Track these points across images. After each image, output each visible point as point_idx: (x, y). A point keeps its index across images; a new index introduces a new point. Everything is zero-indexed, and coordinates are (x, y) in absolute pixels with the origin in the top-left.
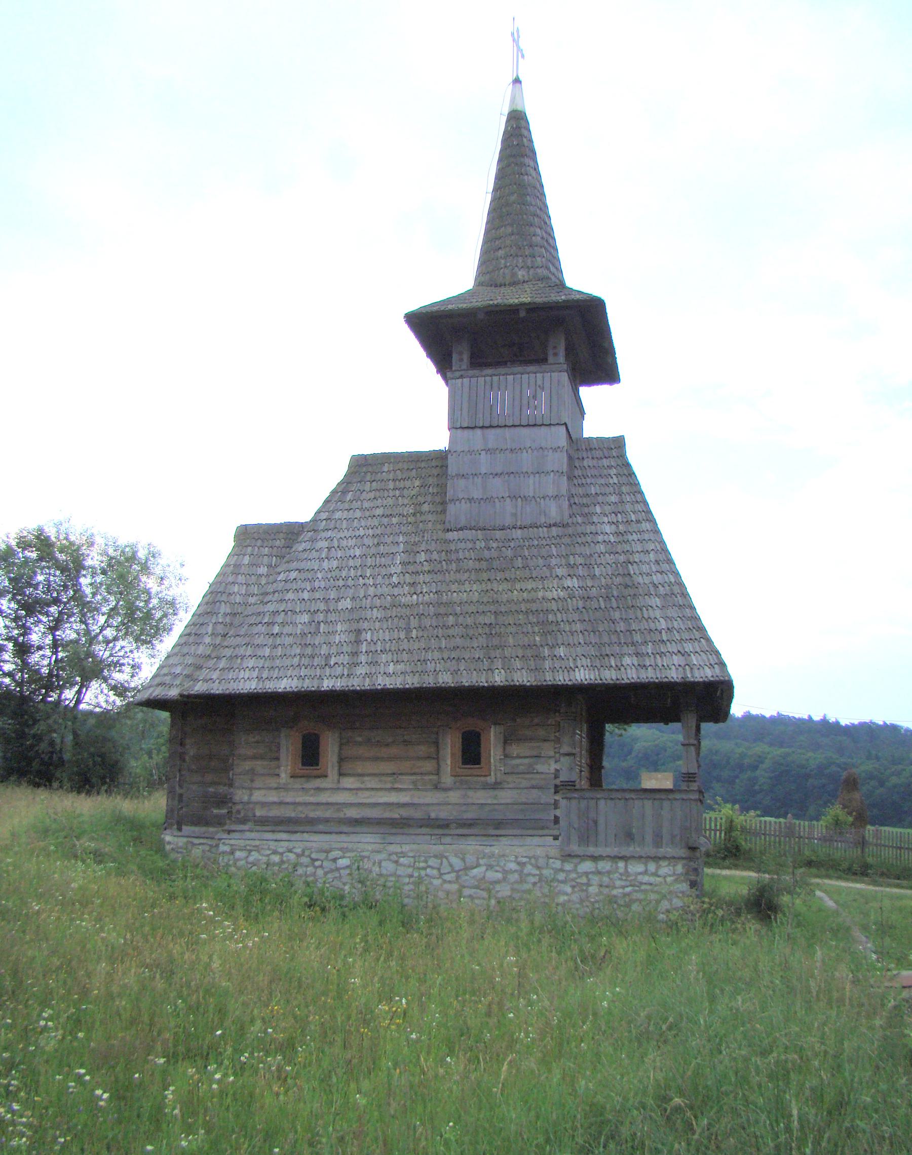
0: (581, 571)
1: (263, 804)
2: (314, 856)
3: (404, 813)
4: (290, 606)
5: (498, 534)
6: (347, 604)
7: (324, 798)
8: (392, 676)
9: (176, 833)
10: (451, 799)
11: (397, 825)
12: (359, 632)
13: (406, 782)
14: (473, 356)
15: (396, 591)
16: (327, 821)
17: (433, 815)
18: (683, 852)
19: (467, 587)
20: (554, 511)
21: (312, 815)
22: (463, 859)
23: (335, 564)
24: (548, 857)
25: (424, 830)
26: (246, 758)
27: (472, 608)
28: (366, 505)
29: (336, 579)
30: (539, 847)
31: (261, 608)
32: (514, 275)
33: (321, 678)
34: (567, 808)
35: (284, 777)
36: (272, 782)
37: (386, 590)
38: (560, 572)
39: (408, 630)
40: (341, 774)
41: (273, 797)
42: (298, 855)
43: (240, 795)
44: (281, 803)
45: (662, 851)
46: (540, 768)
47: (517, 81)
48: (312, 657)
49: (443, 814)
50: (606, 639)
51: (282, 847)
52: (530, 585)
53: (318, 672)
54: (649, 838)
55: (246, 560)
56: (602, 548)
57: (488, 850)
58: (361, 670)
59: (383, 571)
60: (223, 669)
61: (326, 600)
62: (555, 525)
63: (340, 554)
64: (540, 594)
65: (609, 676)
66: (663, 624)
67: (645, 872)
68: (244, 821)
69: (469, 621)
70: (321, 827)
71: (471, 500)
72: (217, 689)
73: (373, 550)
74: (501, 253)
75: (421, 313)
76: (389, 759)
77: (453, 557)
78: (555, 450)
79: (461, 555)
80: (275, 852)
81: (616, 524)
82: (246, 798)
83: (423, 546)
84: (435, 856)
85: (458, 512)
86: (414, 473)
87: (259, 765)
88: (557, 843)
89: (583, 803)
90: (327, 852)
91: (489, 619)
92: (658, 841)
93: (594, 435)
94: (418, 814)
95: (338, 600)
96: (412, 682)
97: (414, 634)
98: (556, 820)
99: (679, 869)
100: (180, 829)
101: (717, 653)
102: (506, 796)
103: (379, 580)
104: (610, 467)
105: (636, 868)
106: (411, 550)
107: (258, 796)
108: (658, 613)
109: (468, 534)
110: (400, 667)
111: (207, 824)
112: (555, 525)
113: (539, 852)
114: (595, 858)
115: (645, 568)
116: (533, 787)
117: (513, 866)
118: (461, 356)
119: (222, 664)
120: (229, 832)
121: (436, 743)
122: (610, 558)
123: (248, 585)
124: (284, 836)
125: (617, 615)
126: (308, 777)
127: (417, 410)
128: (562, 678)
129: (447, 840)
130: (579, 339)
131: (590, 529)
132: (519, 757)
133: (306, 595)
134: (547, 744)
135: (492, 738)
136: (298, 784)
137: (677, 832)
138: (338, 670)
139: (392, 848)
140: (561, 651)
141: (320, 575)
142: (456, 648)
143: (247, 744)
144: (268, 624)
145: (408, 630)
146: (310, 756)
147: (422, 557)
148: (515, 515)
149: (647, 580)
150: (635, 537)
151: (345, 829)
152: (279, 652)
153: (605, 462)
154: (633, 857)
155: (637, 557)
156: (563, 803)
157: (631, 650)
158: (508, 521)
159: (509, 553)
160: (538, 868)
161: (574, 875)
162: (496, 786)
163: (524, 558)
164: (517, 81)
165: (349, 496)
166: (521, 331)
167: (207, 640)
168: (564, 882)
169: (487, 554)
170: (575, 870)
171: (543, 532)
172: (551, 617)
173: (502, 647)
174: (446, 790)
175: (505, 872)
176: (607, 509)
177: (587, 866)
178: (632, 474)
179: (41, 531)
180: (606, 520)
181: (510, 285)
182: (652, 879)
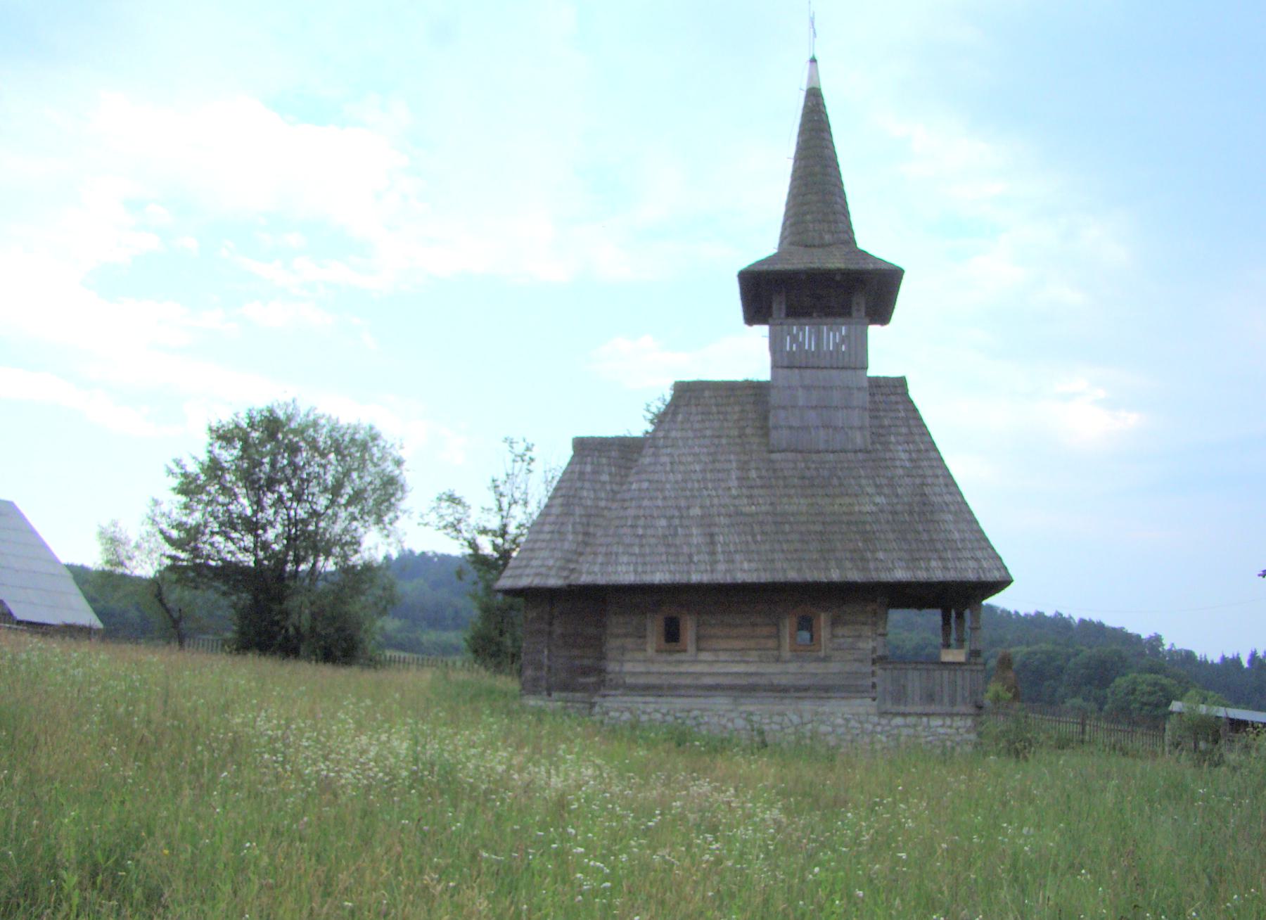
0: (886, 490)
1: (633, 674)
2: (678, 715)
3: (751, 680)
4: (648, 512)
5: (814, 457)
6: (696, 511)
7: (684, 668)
8: (746, 572)
9: (546, 697)
10: (789, 671)
11: (748, 689)
12: (712, 535)
13: (753, 655)
14: (788, 308)
15: (737, 502)
16: (688, 687)
17: (775, 682)
18: (972, 710)
19: (795, 500)
20: (859, 439)
21: (674, 682)
22: (801, 717)
23: (679, 477)
24: (868, 714)
25: (770, 694)
26: (618, 636)
27: (804, 519)
28: (697, 426)
29: (683, 489)
30: (863, 706)
31: (622, 513)
32: (822, 238)
33: (689, 572)
34: (883, 676)
35: (650, 651)
36: (640, 656)
37: (727, 501)
38: (870, 490)
39: (754, 535)
40: (699, 649)
41: (640, 668)
42: (664, 715)
43: (612, 667)
44: (648, 673)
45: (955, 710)
46: (861, 645)
47: (813, 61)
48: (677, 555)
49: (784, 681)
50: (914, 546)
51: (650, 708)
52: (847, 500)
53: (685, 568)
54: (946, 699)
55: (588, 468)
56: (900, 472)
57: (820, 709)
58: (721, 567)
59: (723, 485)
60: (602, 564)
61: (679, 508)
62: (860, 451)
63: (682, 468)
64: (857, 508)
65: (922, 576)
66: (957, 536)
67: (942, 726)
68: (616, 687)
69: (803, 528)
70: (683, 692)
71: (791, 428)
72: (601, 580)
73: (710, 467)
74: (809, 217)
75: (768, 273)
76: (737, 637)
77: (780, 474)
78: (859, 389)
79: (786, 473)
80: (644, 712)
81: (910, 452)
82: (617, 669)
83: (753, 465)
84: (778, 714)
85: (780, 437)
86: (732, 400)
87: (629, 642)
88: (875, 703)
89: (896, 672)
90: (689, 711)
91: (819, 528)
92: (953, 702)
93: (881, 374)
94: (763, 681)
95: (688, 508)
96: (765, 577)
97: (759, 538)
98: (874, 686)
99: (969, 722)
100: (550, 695)
101: (999, 558)
102: (834, 667)
103: (720, 492)
104: (897, 403)
105: (936, 722)
106: (744, 467)
107: (628, 667)
108: (951, 527)
109: (790, 456)
110: (753, 565)
111: (574, 690)
112: (860, 451)
113: (862, 710)
114: (904, 715)
115: (937, 489)
116: (855, 660)
117: (840, 721)
118: (779, 307)
119: (600, 559)
120: (604, 696)
121: (777, 625)
122: (907, 480)
123: (595, 490)
124: (651, 699)
125: (920, 528)
126: (670, 652)
127: (744, 353)
128: (885, 577)
129: (787, 701)
130: (867, 291)
131: (888, 455)
132: (843, 636)
133: (660, 503)
134: (866, 628)
135: (822, 625)
136: (665, 657)
137: (967, 694)
138: (702, 567)
139: (742, 708)
140: (881, 555)
141: (668, 486)
142: (796, 551)
143: (617, 624)
144: (632, 526)
145: (754, 535)
146: (672, 634)
147: (753, 474)
148: (827, 441)
149: (939, 499)
150: (925, 463)
151: (700, 692)
152: (647, 550)
153: (893, 398)
154: (933, 714)
155: (929, 480)
156: (879, 672)
157: (935, 556)
158: (822, 446)
159: (826, 473)
160: (861, 722)
161: (888, 728)
162: (826, 659)
163: (839, 478)
164: (813, 61)
165: (680, 417)
166: (819, 284)
167: (570, 537)
168: (881, 733)
169: (807, 474)
170: (889, 724)
171: (851, 456)
172: (868, 528)
173: (833, 551)
174: (786, 662)
175: (834, 726)
176: (901, 439)
177: (898, 721)
178: (915, 410)
179: (272, 411)
180: (900, 448)
181: (819, 246)
182: (949, 731)
